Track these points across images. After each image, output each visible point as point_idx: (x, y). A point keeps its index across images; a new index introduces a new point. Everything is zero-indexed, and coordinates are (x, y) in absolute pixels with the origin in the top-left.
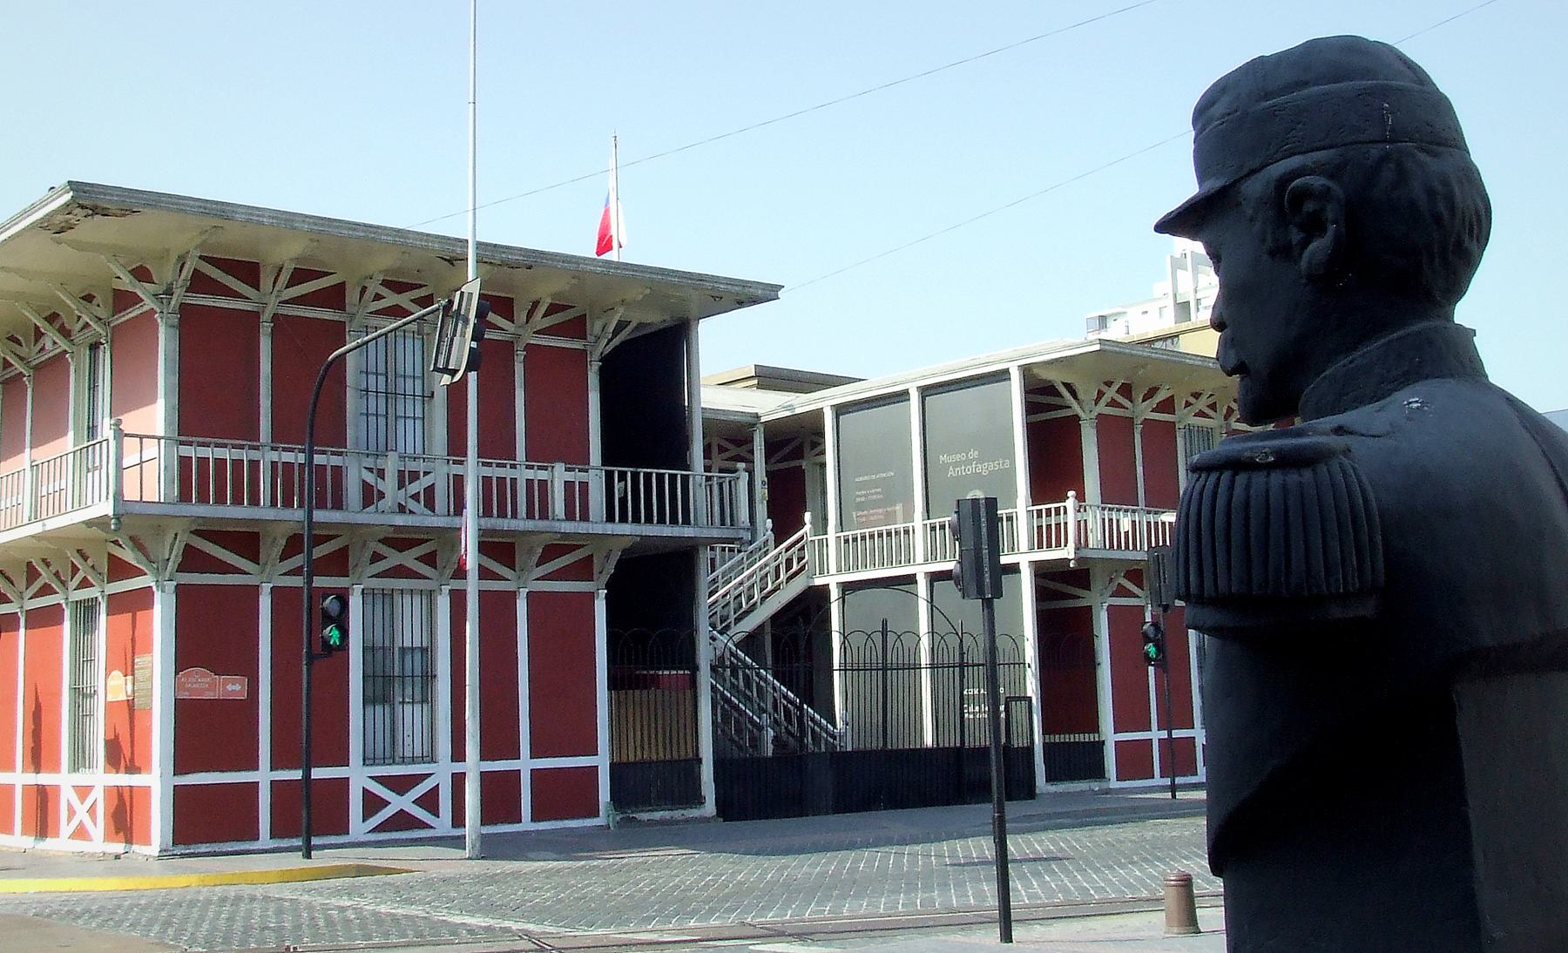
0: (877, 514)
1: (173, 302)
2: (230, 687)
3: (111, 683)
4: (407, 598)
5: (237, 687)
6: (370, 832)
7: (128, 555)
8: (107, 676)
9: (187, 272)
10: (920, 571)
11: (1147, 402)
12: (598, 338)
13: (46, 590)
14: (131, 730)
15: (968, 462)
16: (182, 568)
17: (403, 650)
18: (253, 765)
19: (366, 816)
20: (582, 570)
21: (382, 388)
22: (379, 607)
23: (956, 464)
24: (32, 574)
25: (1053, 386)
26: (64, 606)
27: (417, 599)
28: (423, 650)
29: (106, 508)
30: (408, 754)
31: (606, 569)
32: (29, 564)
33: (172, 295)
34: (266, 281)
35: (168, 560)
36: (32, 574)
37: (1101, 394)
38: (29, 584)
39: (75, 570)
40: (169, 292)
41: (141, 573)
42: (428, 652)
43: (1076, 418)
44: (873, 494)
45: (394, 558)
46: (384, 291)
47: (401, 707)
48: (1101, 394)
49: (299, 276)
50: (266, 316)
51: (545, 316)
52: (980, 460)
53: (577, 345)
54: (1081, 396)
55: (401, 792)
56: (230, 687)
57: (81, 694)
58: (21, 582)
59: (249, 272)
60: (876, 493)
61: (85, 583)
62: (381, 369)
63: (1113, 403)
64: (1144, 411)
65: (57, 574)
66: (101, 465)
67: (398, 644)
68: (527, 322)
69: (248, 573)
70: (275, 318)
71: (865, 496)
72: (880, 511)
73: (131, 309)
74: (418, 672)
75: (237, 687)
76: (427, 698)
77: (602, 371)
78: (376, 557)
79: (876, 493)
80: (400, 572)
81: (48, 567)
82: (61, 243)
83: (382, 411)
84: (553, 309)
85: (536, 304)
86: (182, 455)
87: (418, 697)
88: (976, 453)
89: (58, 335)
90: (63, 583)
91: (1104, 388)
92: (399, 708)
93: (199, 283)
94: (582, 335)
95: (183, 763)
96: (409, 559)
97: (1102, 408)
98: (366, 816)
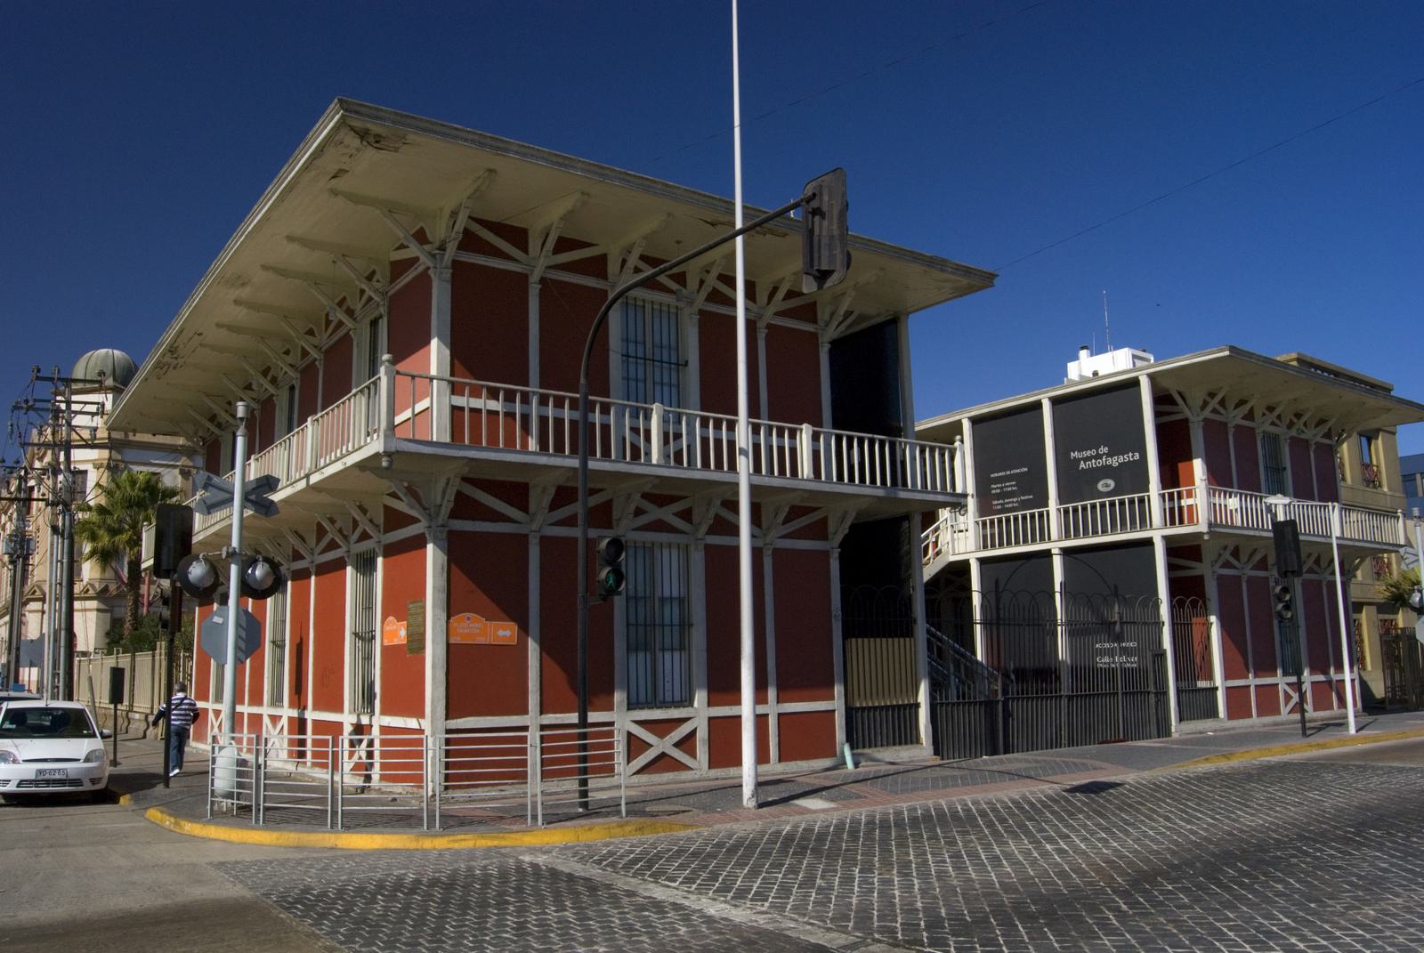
0: (1013, 502)
1: (446, 257)
2: (501, 633)
3: (387, 628)
4: (666, 552)
5: (508, 633)
6: (634, 774)
7: (402, 506)
8: (383, 622)
9: (459, 227)
10: (1055, 547)
11: (1239, 409)
12: (827, 324)
13: (333, 545)
14: (1080, 398)
15: (1099, 456)
16: (454, 515)
17: (662, 600)
18: (523, 710)
19: (630, 757)
20: (819, 530)
21: (640, 354)
22: (640, 560)
23: (1086, 459)
24: (321, 532)
25: (1171, 395)
26: (346, 559)
27: (675, 553)
28: (681, 601)
29: (376, 446)
30: (668, 699)
31: (838, 532)
32: (319, 525)
33: (444, 250)
34: (534, 244)
35: (441, 505)
36: (321, 532)
37: (1205, 404)
38: (319, 540)
39: (355, 524)
40: (442, 248)
41: (415, 521)
42: (683, 602)
43: (1186, 421)
44: (1007, 487)
45: (655, 513)
46: (642, 265)
47: (661, 654)
48: (1205, 404)
49: (564, 245)
50: (535, 278)
51: (784, 299)
52: (1109, 455)
53: (808, 327)
54: (1190, 401)
55: (661, 735)
56: (501, 633)
57: (366, 637)
58: (312, 540)
59: (518, 237)
60: (1011, 486)
61: (365, 536)
62: (640, 338)
63: (1214, 411)
64: (1235, 418)
65: (340, 531)
66: (379, 427)
67: (658, 594)
68: (768, 303)
69: (516, 520)
70: (543, 281)
71: (1001, 488)
72: (1015, 500)
73: (462, 837)
74: (676, 621)
75: (508, 633)
76: (683, 646)
77: (831, 351)
78: (639, 512)
79: (1011, 486)
80: (659, 526)
81: (333, 524)
82: (337, 195)
83: (641, 376)
84: (791, 294)
85: (775, 290)
86: (454, 404)
87: (676, 644)
88: (1106, 449)
89: (344, 314)
90: (346, 538)
91: (1208, 399)
92: (659, 655)
93: (469, 241)
94: (814, 321)
95: (453, 708)
96: (667, 514)
97: (1207, 413)
98: (630, 757)
